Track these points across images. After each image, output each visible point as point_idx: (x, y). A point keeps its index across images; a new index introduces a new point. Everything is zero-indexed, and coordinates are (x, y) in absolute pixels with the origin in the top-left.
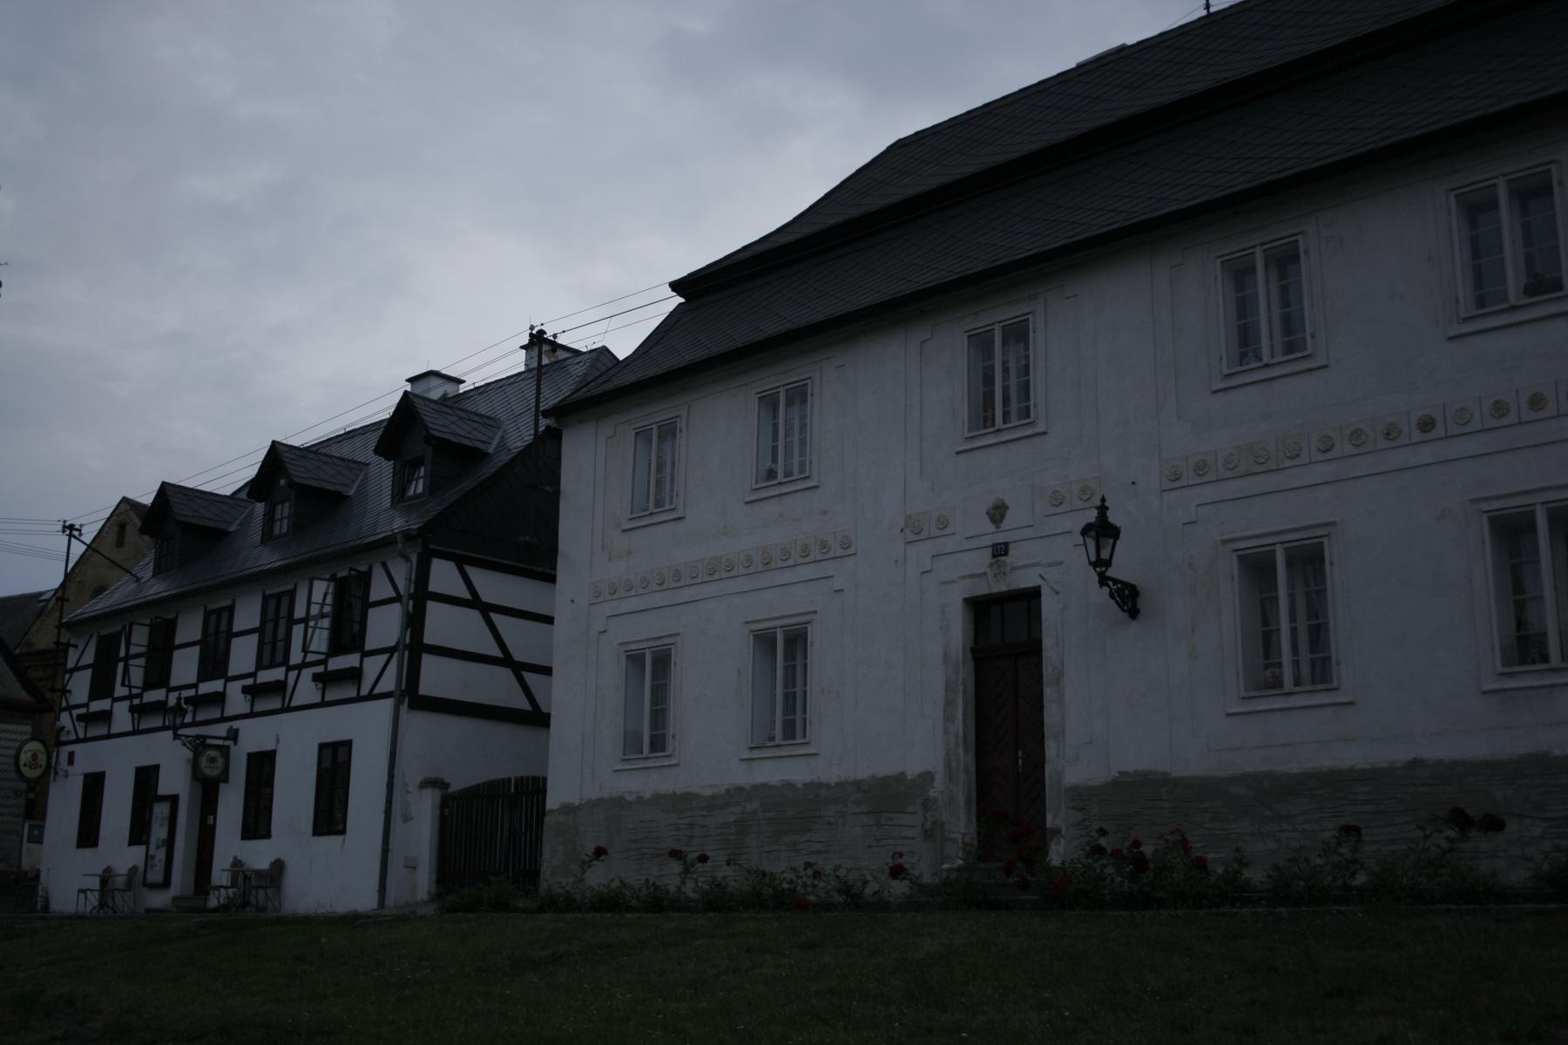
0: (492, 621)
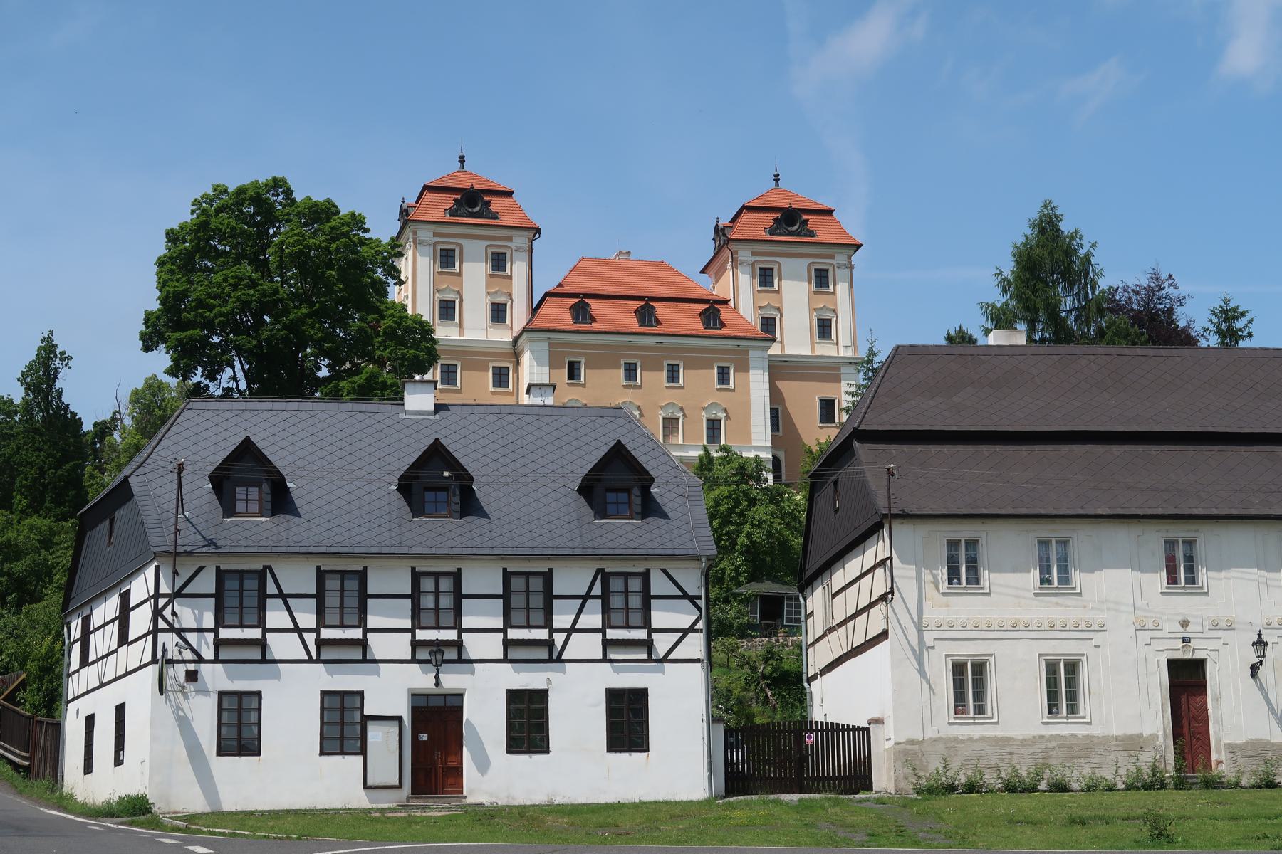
0: (163, 607)
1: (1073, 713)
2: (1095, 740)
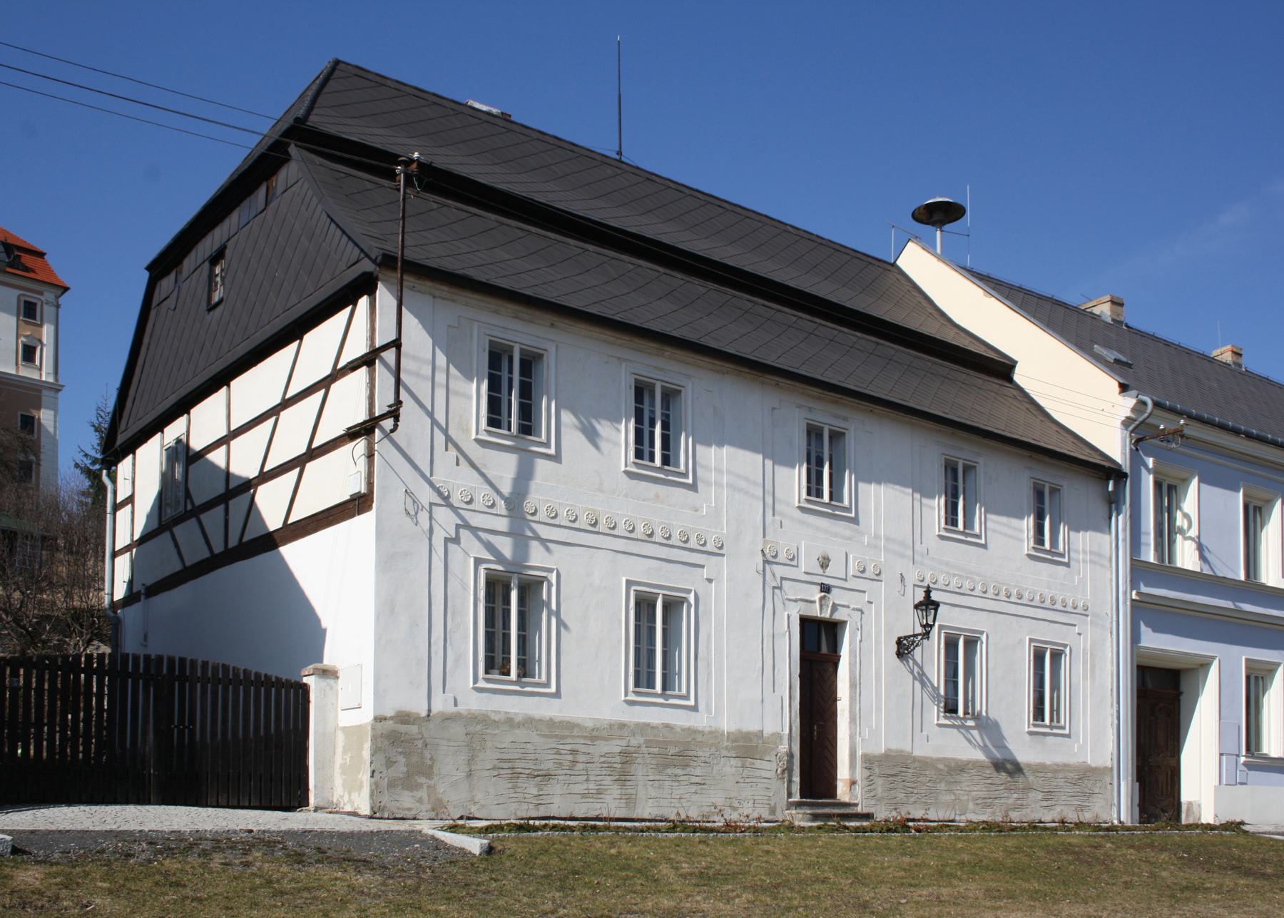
1: (648, 687)
2: (699, 738)
